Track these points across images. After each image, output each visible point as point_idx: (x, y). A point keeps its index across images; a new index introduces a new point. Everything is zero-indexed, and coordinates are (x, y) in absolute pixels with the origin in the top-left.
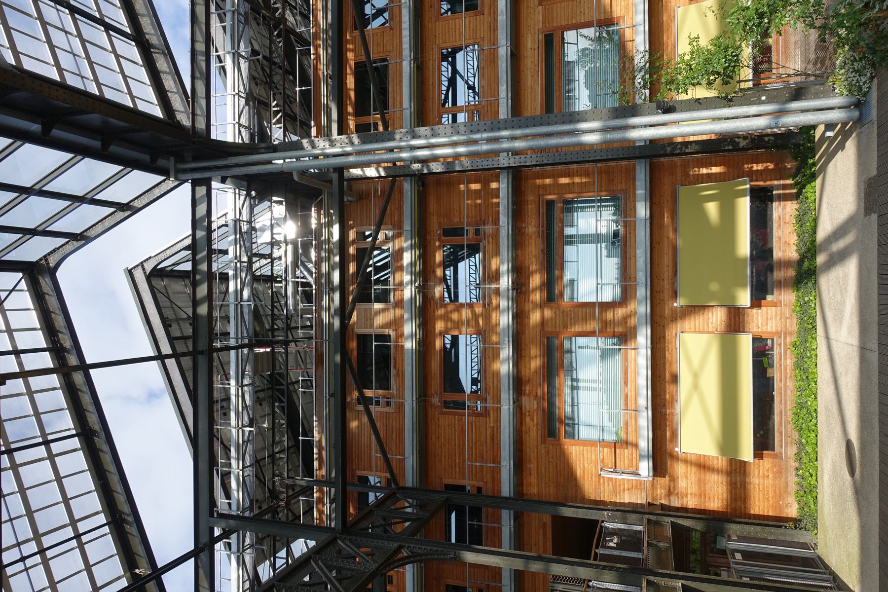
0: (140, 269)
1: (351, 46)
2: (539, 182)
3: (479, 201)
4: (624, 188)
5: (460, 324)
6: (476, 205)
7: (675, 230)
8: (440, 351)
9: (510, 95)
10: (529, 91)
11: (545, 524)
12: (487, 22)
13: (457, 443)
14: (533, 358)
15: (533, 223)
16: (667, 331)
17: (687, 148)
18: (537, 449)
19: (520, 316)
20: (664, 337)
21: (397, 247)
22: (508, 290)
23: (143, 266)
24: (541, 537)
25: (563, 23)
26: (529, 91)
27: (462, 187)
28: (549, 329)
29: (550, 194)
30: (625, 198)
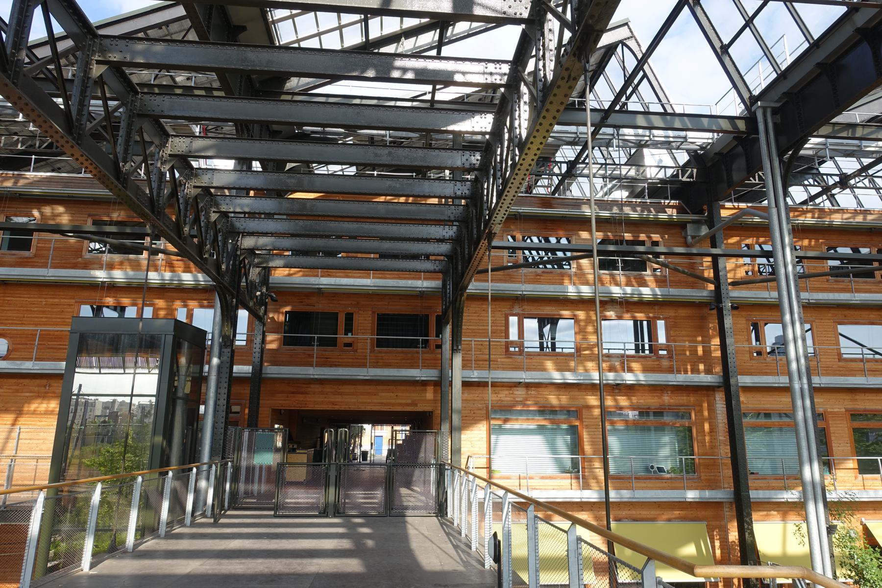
0: (629, 34)
1: (813, 243)
2: (705, 405)
3: (688, 353)
4: (702, 478)
5: (584, 334)
6: (685, 351)
7: (669, 520)
8: (560, 315)
9: (781, 385)
10: (779, 399)
11: (416, 405)
12: (833, 365)
13: (481, 327)
14: (558, 398)
15: (672, 401)
16: (588, 513)
17: (749, 534)
18: (481, 400)
19: (593, 388)
20: (583, 510)
21: (647, 278)
22: (623, 380)
23: (632, 37)
24: (404, 401)
25: (831, 429)
26: (779, 399)
27: (700, 339)
28: (585, 412)
29: (696, 416)
30: (694, 479)
